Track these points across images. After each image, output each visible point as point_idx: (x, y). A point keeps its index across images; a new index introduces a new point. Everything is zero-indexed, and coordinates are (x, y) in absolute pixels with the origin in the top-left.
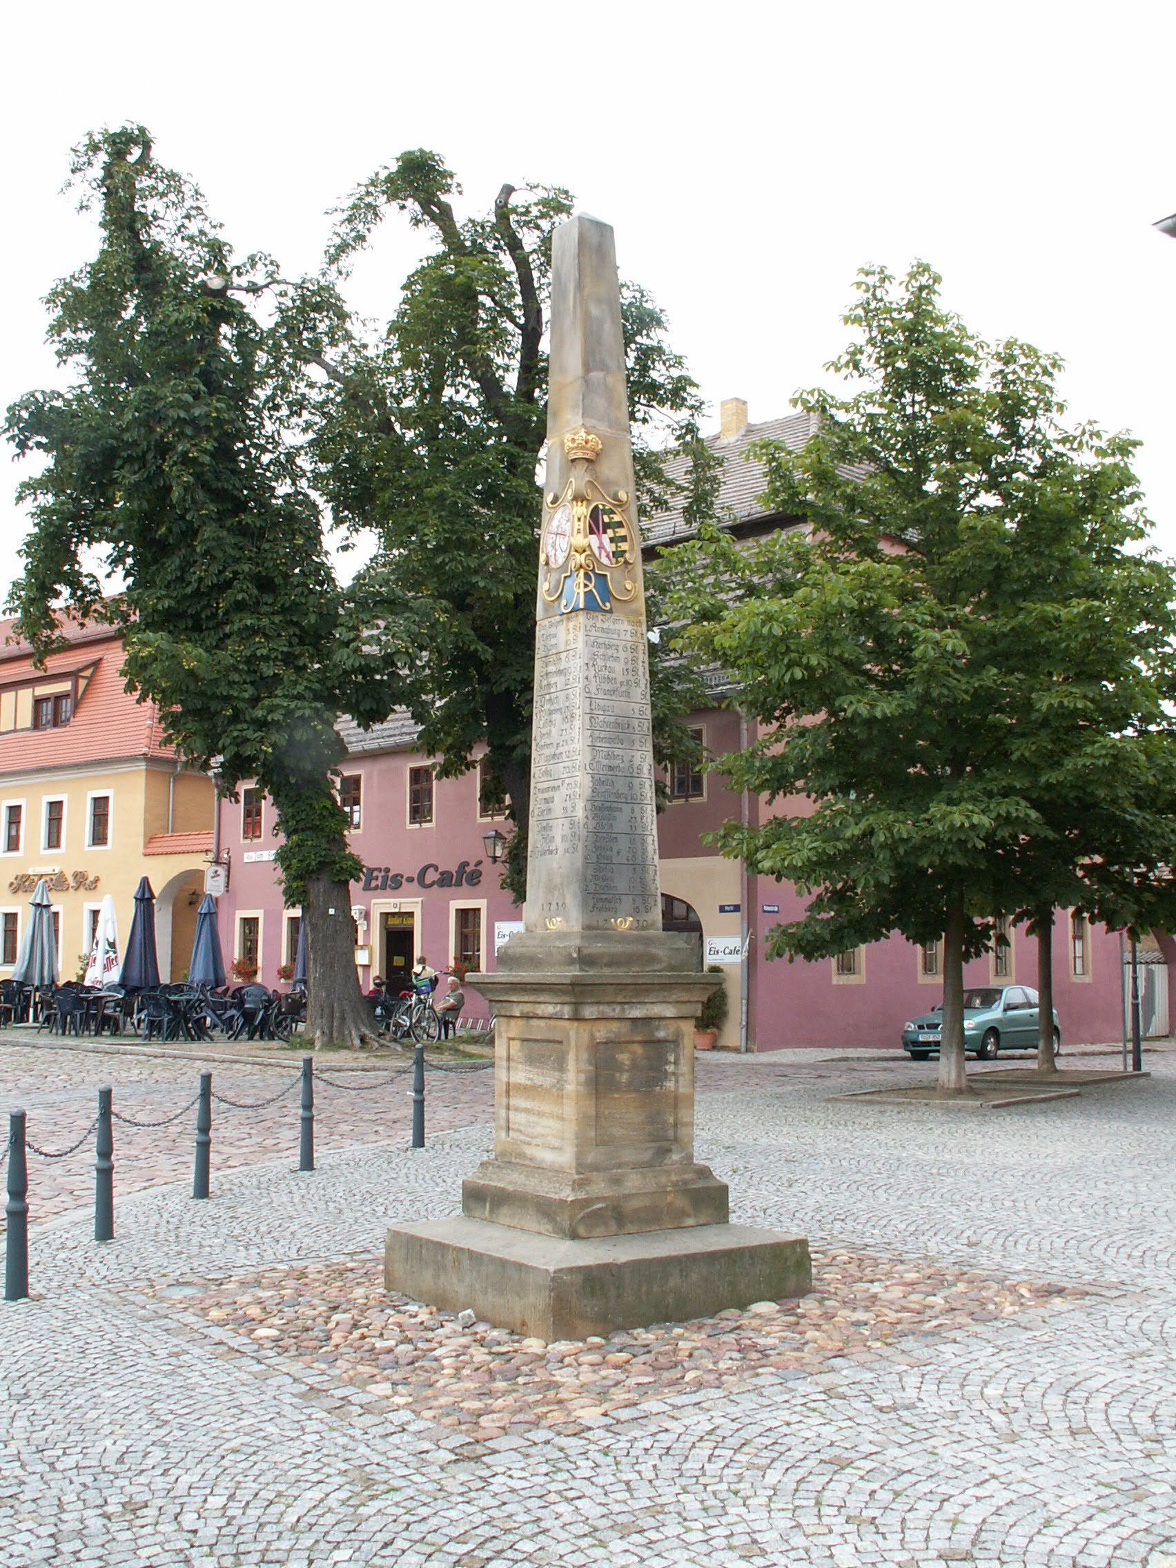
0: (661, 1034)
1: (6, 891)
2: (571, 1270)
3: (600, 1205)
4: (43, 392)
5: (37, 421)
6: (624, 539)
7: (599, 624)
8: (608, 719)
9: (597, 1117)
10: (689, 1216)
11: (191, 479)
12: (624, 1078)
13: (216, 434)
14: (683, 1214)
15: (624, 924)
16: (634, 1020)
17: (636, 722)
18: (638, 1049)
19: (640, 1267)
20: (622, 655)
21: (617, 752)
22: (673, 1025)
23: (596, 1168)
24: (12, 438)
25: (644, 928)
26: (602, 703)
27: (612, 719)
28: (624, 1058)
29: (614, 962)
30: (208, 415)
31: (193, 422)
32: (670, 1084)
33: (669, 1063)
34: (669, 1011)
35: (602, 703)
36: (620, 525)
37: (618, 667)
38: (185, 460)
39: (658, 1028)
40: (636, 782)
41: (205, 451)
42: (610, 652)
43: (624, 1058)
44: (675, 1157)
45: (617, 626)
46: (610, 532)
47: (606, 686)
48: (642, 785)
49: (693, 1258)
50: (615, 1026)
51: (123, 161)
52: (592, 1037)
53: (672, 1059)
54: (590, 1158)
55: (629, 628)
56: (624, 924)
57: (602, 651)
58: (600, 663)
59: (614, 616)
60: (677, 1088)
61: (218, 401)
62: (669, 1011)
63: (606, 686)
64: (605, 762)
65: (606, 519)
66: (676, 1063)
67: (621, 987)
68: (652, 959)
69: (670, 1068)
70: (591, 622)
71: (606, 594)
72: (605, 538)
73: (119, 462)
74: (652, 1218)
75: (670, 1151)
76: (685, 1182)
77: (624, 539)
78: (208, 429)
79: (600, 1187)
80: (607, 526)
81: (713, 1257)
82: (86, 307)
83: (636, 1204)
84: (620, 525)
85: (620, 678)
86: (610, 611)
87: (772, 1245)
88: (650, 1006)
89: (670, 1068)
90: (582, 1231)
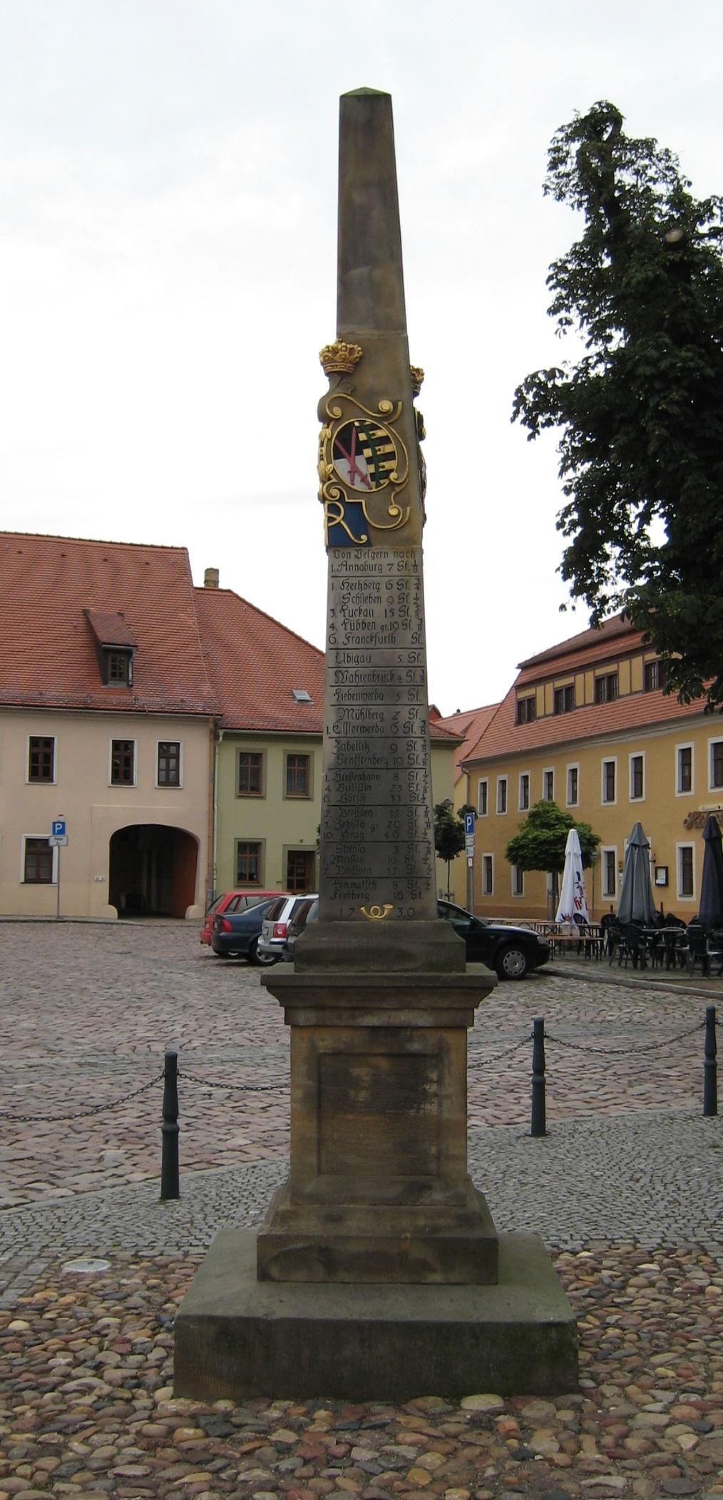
0: (415, 1047)
1: (682, 827)
2: (200, 1319)
3: (300, 1245)
4: (545, 372)
5: (541, 400)
6: (390, 456)
7: (352, 561)
8: (361, 671)
9: (320, 1143)
10: (434, 1270)
11: (664, 431)
12: (363, 1096)
13: (685, 383)
14: (424, 1266)
15: (379, 913)
16: (374, 1029)
17: (403, 672)
18: (384, 1064)
19: (297, 1327)
20: (384, 594)
21: (374, 709)
22: (433, 1038)
23: (315, 1198)
24: (523, 422)
25: (411, 918)
26: (353, 653)
27: (368, 671)
28: (362, 1072)
29: (343, 958)
30: (673, 366)
31: (662, 375)
32: (431, 1108)
33: (428, 1081)
34: (423, 1020)
35: (353, 653)
36: (385, 440)
37: (379, 609)
38: (661, 416)
39: (410, 1039)
40: (402, 744)
41: (673, 402)
42: (366, 592)
43: (362, 1072)
44: (437, 1196)
45: (377, 561)
46: (368, 452)
47: (361, 633)
48: (411, 746)
49: (382, 1327)
50: (345, 1036)
51: (598, 134)
52: (313, 1046)
53: (434, 1076)
54: (309, 1187)
55: (396, 561)
56: (379, 913)
57: (354, 593)
58: (351, 606)
59: (373, 549)
60: (440, 1112)
61: (688, 350)
62: (423, 1020)
63: (361, 633)
64: (356, 722)
65: (362, 437)
66: (439, 1082)
67: (339, 991)
68: (404, 956)
69: (432, 1088)
70: (340, 561)
71: (360, 524)
72: (360, 461)
73: (615, 426)
74: (383, 1265)
75: (430, 1188)
76: (435, 1229)
77: (390, 456)
78: (678, 381)
79: (310, 1226)
80: (361, 446)
81: (411, 1329)
82: (578, 284)
83: (353, 1248)
84: (385, 440)
85: (381, 621)
86: (368, 544)
87: (508, 1326)
88: (393, 1014)
89: (432, 1088)
90: (274, 1271)
